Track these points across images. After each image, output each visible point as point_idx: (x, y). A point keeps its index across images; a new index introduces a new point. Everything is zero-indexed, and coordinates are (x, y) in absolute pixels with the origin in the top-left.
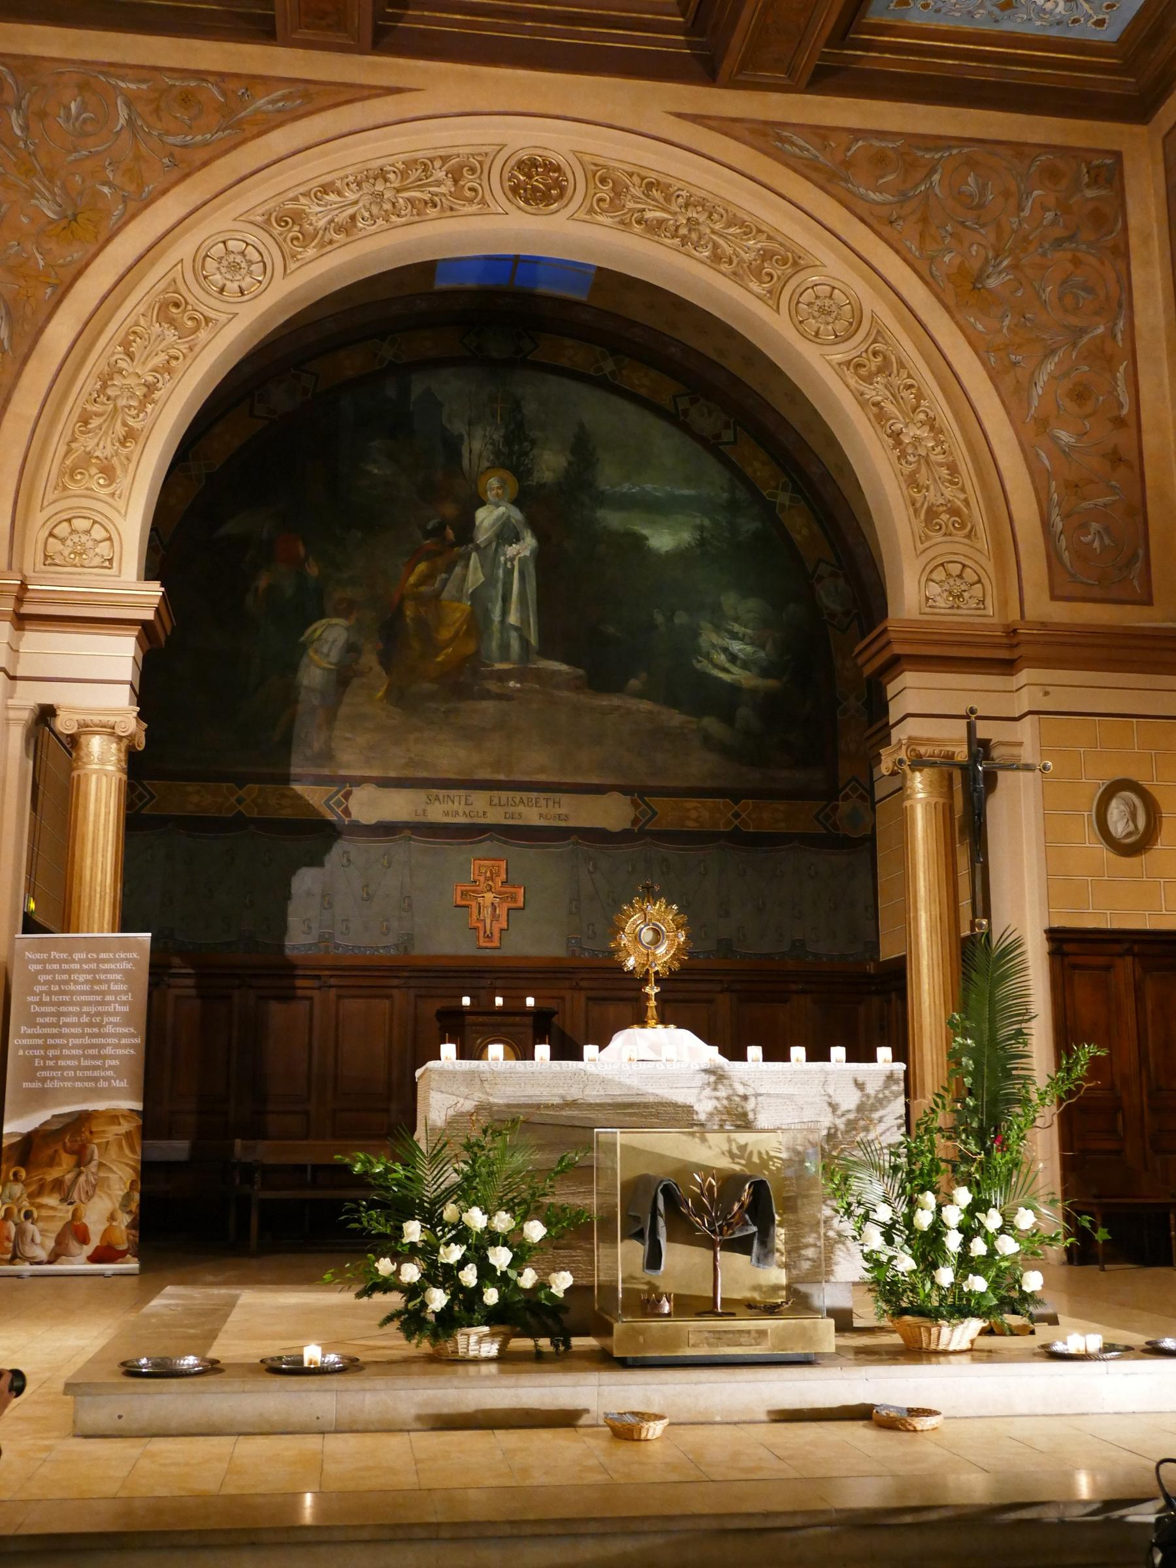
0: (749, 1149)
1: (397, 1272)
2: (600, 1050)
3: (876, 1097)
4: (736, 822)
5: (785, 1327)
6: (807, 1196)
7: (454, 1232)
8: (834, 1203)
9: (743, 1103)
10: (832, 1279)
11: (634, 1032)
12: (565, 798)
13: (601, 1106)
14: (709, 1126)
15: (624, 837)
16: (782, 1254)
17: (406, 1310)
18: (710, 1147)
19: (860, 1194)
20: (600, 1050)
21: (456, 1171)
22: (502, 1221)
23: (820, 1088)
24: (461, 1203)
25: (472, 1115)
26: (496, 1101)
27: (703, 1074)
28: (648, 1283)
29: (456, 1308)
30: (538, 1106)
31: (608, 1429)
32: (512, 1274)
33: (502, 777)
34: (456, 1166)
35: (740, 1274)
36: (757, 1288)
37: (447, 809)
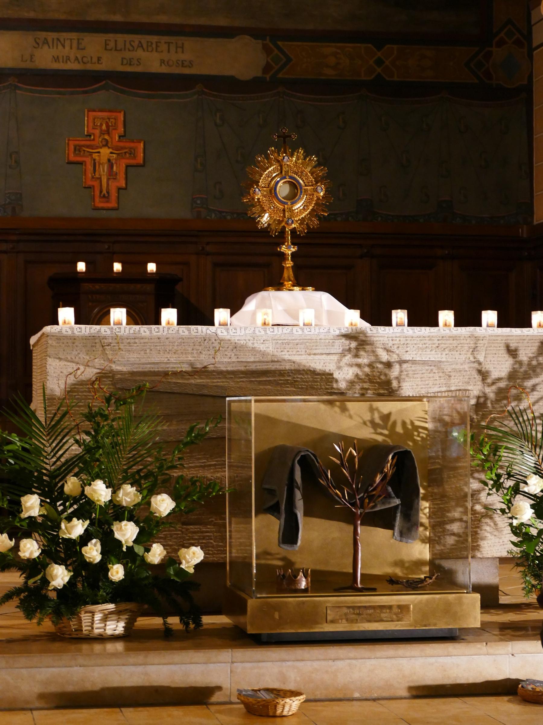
0: (392, 418)
1: (16, 548)
2: (232, 314)
3: (529, 364)
4: (379, 70)
5: (427, 601)
6: (455, 469)
7: (75, 507)
8: (483, 476)
9: (387, 371)
10: (479, 555)
11: (270, 295)
12: (189, 43)
13: (234, 373)
14: (350, 393)
15: (254, 86)
16: (426, 528)
17: (25, 588)
18: (351, 417)
19: (510, 466)
20: (232, 314)
21: (77, 442)
22: (127, 494)
23: (469, 355)
24: (84, 477)
25: (93, 383)
26: (119, 368)
27: (343, 340)
28: (284, 559)
29: (80, 586)
30: (166, 374)
31: (242, 706)
32: (139, 550)
33: (118, 18)
34: (78, 437)
35: (381, 548)
36: (400, 563)
37: (56, 54)
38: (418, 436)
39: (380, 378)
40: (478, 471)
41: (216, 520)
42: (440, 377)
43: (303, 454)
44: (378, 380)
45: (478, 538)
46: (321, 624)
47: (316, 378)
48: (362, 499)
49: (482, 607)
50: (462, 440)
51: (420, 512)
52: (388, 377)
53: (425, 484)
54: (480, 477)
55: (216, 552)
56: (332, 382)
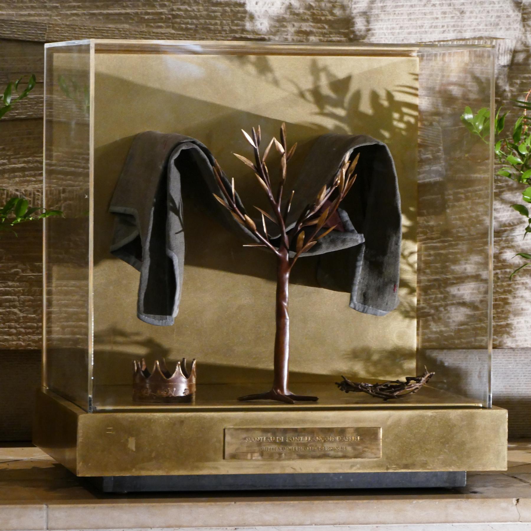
0: (354, 87)
5: (410, 424)
10: (509, 342)
16: (412, 291)
18: (276, 82)
28: (149, 343)
35: (327, 328)
36: (361, 354)
38: (401, 120)
39: (332, 14)
40: (511, 189)
41: (23, 271)
42: (445, 13)
43: (184, 148)
44: (330, 17)
45: (509, 312)
46: (214, 460)
47: (214, 12)
48: (293, 234)
49: (512, 438)
50: (481, 127)
51: (401, 260)
52: (348, 12)
53: (412, 209)
54: (514, 200)
55: (23, 330)
56: (242, 19)
